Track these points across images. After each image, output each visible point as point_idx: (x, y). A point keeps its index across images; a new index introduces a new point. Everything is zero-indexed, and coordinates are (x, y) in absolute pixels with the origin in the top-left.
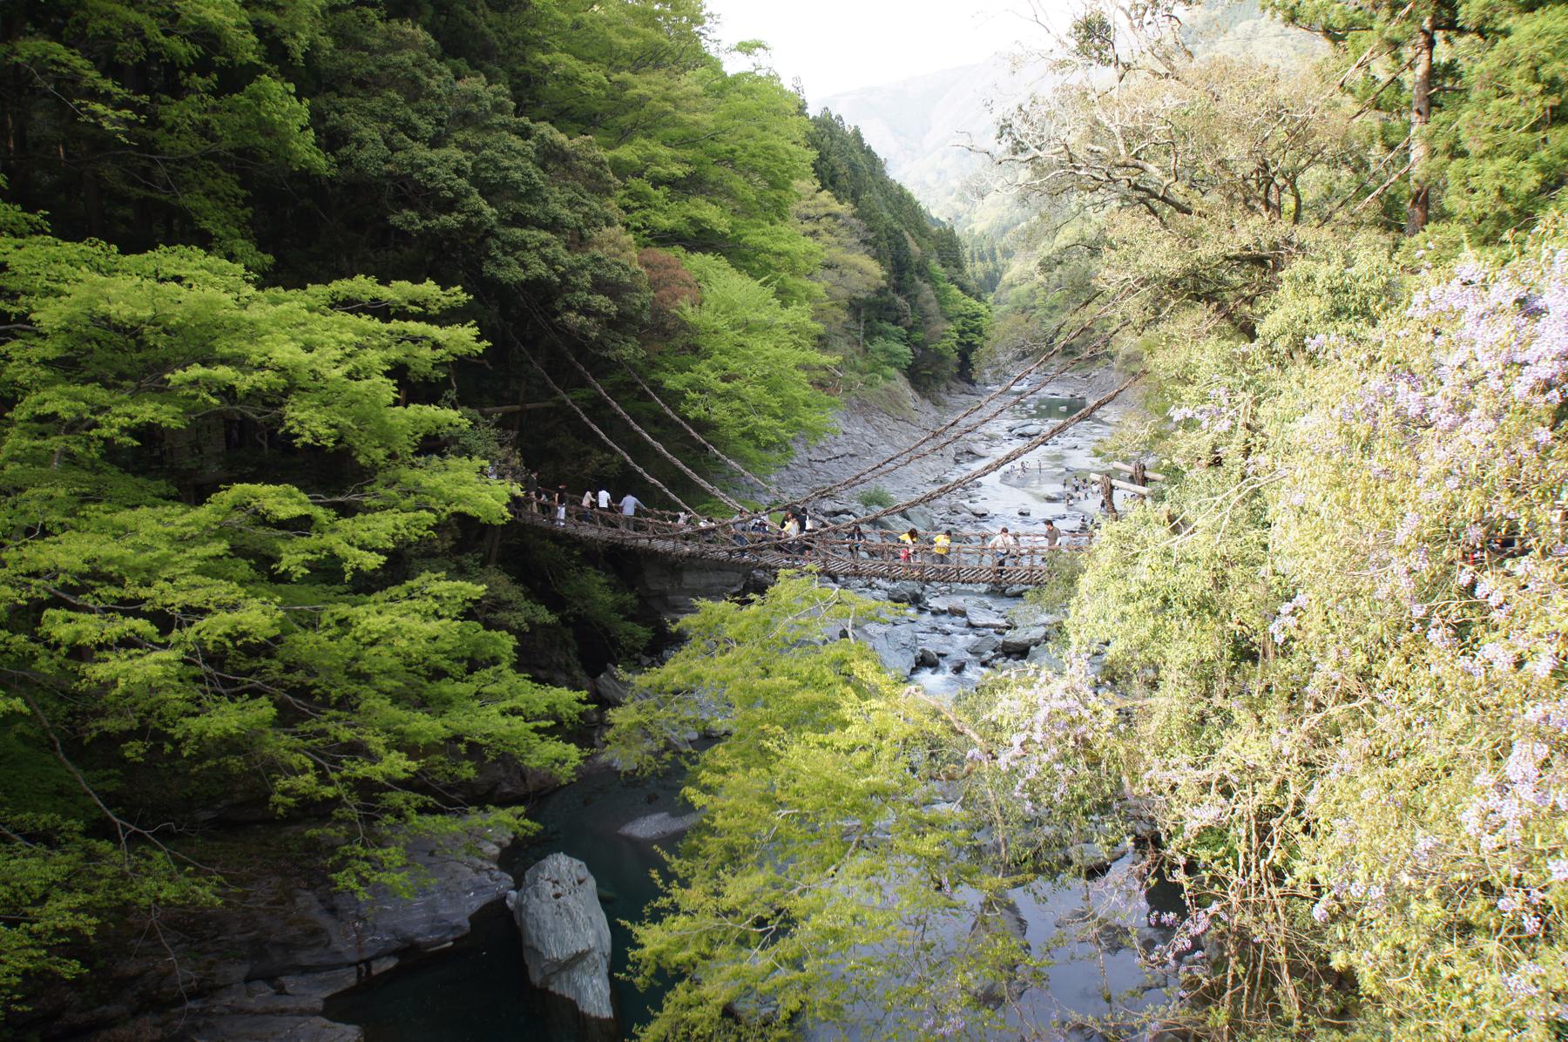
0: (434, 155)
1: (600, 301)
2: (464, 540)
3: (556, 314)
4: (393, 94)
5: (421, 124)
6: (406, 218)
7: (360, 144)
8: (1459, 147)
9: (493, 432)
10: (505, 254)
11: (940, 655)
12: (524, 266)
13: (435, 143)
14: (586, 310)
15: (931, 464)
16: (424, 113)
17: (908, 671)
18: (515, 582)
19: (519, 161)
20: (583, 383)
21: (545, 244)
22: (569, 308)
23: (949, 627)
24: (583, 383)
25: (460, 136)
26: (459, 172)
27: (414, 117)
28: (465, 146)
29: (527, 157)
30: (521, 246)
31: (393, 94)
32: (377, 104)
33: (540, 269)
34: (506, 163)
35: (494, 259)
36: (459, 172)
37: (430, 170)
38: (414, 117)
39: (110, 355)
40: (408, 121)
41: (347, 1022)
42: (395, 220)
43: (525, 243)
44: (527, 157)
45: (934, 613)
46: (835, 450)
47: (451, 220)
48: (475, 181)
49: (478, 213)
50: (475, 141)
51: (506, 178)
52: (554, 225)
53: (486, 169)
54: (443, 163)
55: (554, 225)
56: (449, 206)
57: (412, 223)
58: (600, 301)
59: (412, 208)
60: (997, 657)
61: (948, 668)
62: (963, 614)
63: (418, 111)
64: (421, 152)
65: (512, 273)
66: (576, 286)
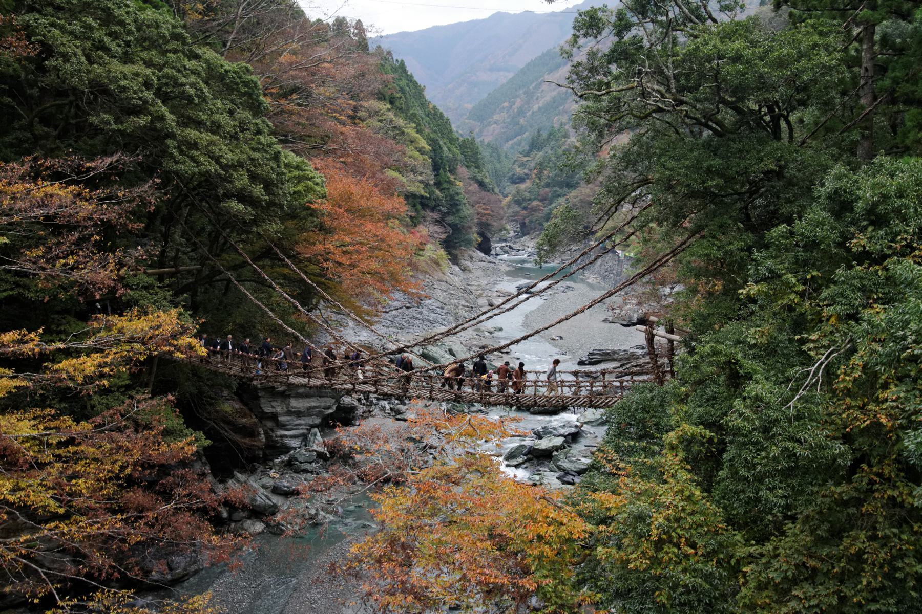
0: (128, 69)
1: (258, 190)
2: (155, 372)
3: (219, 200)
4: (90, 20)
5: (113, 46)
6: (103, 118)
7: (66, 58)
8: (810, 582)
10: (181, 152)
13: (126, 59)
16: (114, 36)
19: (192, 79)
21: (211, 143)
25: (144, 55)
26: (147, 85)
27: (107, 39)
28: (148, 64)
29: (197, 74)
30: (194, 145)
31: (90, 20)
32: (77, 27)
34: (183, 80)
35: (172, 156)
36: (147, 85)
37: (123, 83)
38: (107, 39)
39: (423, 116)
40: (101, 41)
42: (93, 119)
43: (196, 144)
44: (197, 74)
47: (143, 121)
48: (158, 93)
49: (162, 118)
50: (158, 60)
51: (184, 91)
52: (216, 128)
53: (167, 84)
54: (128, 74)
55: (216, 128)
56: (136, 111)
57: (108, 123)
59: (108, 112)
63: (110, 34)
64: (116, 67)
65: (187, 167)
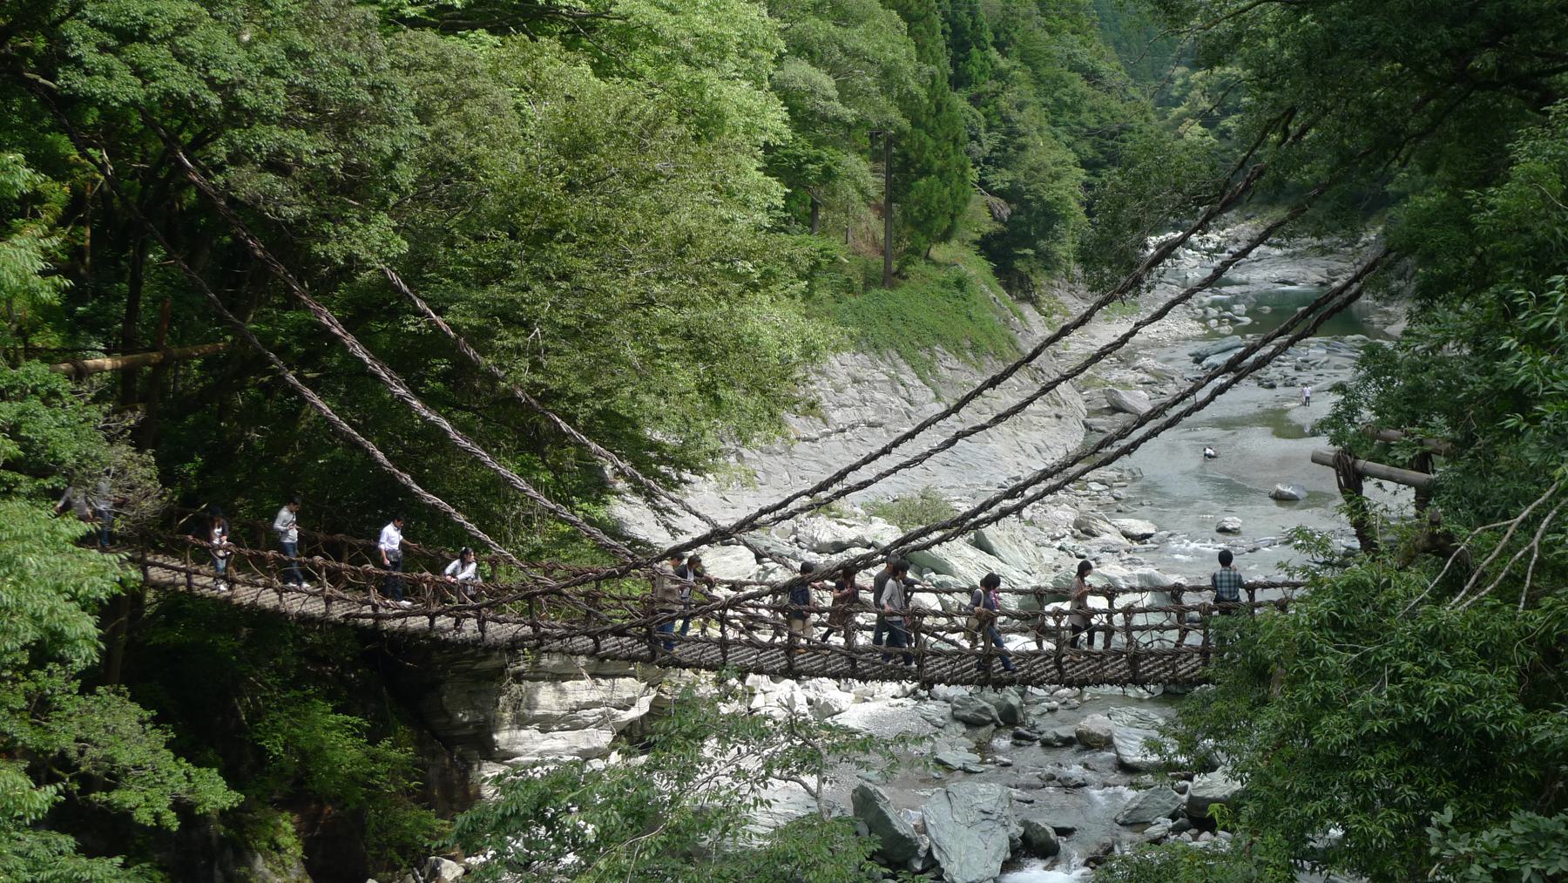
1: (308, 145)
9: (93, 411)
11: (1062, 832)
12: (142, 73)
14: (276, 164)
15: (1037, 437)
17: (996, 866)
18: (157, 722)
20: (292, 302)
22: (237, 158)
23: (1075, 771)
24: (292, 302)
33: (181, 82)
35: (78, 62)
41: (63, 831)
45: (1047, 744)
46: (837, 416)
58: (308, 145)
60: (1177, 830)
61: (1077, 860)
62: (1107, 743)
66: (254, 114)
